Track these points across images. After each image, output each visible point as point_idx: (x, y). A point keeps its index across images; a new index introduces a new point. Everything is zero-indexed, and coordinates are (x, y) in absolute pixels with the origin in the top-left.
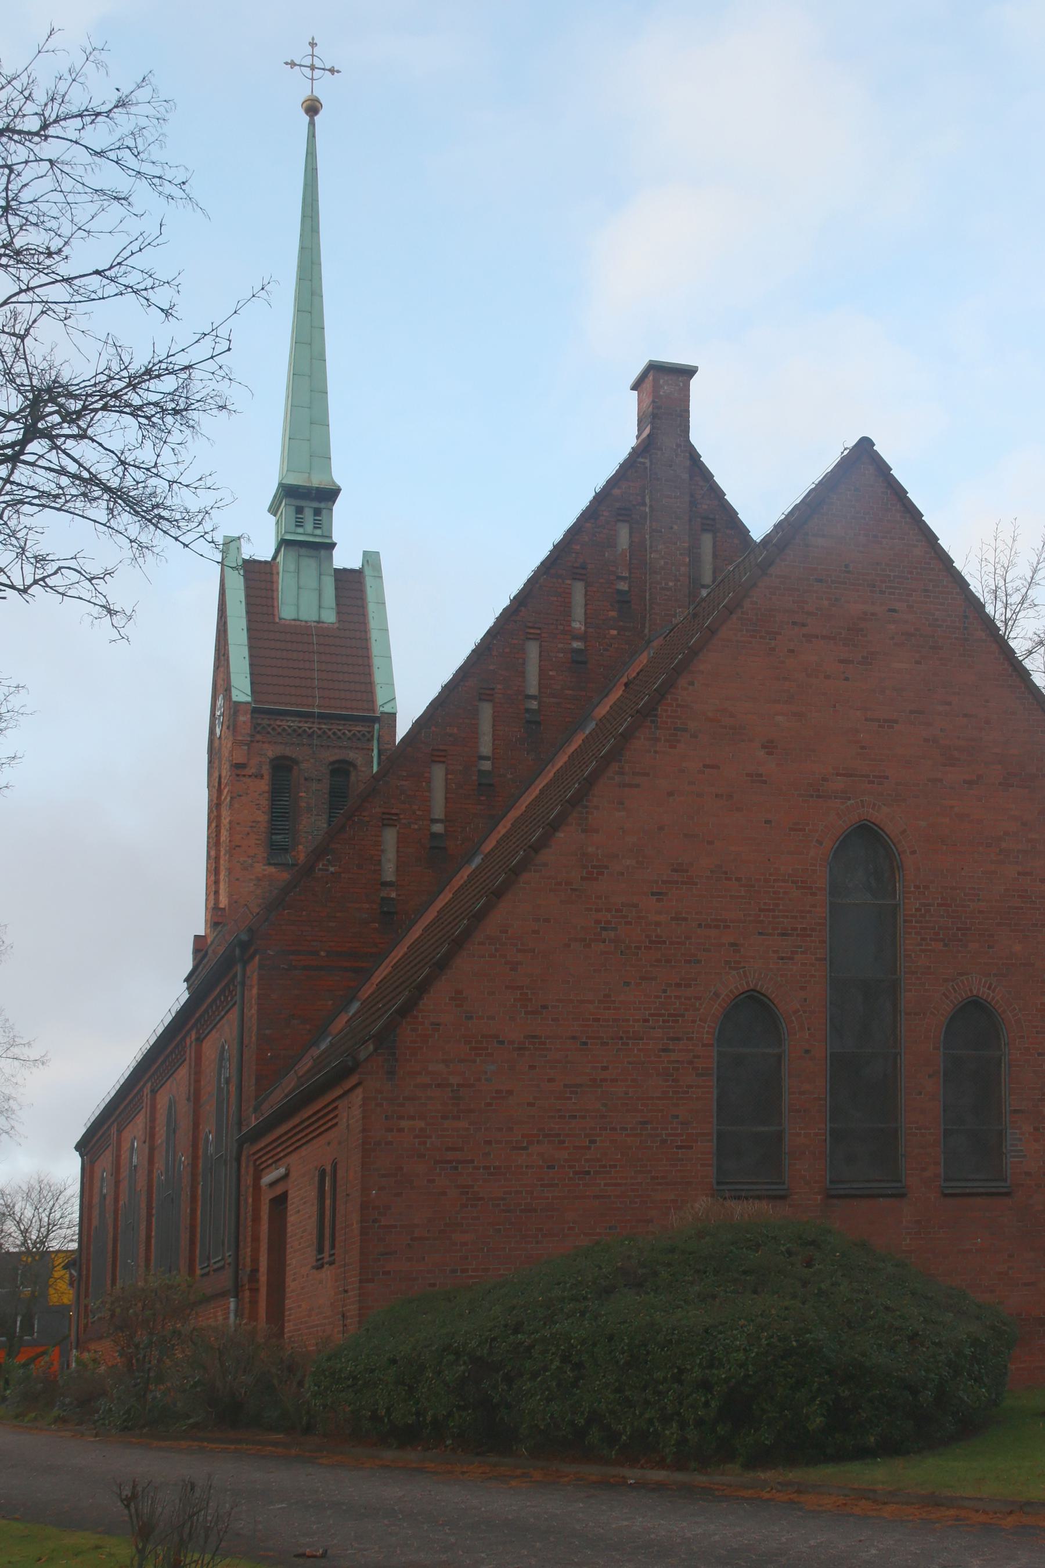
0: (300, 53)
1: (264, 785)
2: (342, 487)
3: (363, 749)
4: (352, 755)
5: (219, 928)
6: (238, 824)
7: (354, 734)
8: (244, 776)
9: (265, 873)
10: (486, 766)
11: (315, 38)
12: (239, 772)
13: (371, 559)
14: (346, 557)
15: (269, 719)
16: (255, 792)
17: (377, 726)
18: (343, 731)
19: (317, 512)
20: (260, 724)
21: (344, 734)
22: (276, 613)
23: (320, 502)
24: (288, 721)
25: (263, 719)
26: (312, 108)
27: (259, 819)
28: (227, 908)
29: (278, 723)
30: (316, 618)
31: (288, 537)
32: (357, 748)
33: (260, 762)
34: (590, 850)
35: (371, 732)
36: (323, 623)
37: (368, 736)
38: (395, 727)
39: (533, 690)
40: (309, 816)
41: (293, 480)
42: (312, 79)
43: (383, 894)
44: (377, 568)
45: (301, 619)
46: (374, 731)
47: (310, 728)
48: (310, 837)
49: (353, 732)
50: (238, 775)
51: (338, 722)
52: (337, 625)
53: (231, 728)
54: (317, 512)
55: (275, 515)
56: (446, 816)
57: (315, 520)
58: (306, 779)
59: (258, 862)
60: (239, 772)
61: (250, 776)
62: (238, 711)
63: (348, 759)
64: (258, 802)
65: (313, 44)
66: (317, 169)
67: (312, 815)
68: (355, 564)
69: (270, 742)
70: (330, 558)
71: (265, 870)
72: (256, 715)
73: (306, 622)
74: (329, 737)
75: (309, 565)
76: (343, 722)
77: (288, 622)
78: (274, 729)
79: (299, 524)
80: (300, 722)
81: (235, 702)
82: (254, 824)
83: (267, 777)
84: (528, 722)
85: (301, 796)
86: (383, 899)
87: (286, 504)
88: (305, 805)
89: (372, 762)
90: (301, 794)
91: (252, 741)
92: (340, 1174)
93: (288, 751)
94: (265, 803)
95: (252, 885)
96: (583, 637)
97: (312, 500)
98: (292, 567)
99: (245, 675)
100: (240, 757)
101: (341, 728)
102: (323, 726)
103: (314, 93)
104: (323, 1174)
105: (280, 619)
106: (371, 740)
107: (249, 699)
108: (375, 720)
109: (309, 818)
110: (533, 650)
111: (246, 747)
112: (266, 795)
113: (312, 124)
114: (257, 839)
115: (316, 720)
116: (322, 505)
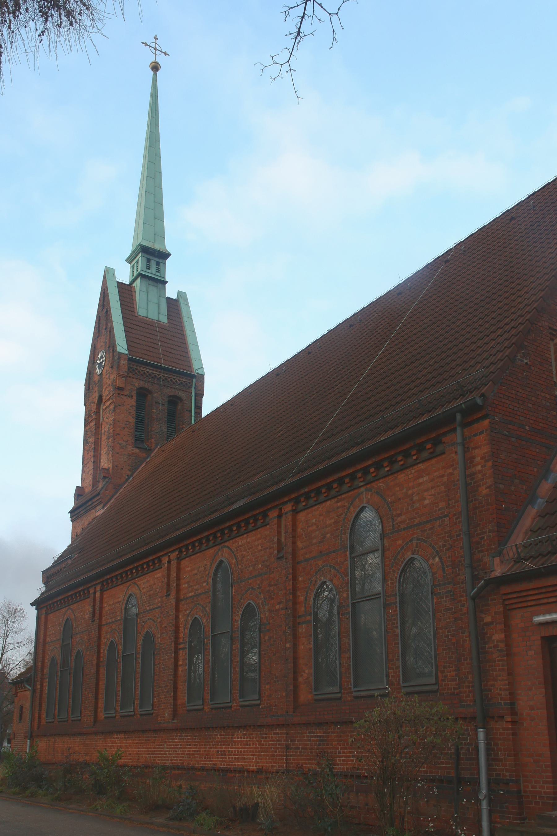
0: (150, 40)
1: (132, 402)
2: (171, 253)
3: (186, 391)
4: (180, 394)
5: (107, 480)
6: (118, 421)
7: (181, 383)
8: (122, 395)
9: (133, 452)
11: (142, 41)
12: (119, 392)
14: (171, 292)
15: (137, 366)
16: (128, 405)
17: (194, 380)
18: (176, 380)
19: (158, 264)
20: (131, 368)
21: (176, 381)
22: (136, 311)
23: (159, 259)
24: (147, 369)
25: (133, 365)
26: (155, 68)
27: (130, 421)
28: (111, 469)
29: (142, 369)
30: (157, 319)
31: (143, 273)
32: (183, 391)
33: (131, 388)
35: (191, 383)
36: (161, 322)
37: (189, 385)
38: (204, 382)
40: (157, 423)
41: (145, 243)
42: (155, 54)
44: (186, 300)
45: (149, 317)
46: (192, 383)
47: (159, 375)
48: (158, 435)
49: (181, 381)
50: (119, 394)
51: (173, 374)
52: (168, 325)
53: (115, 367)
54: (158, 264)
55: (130, 263)
57: (156, 267)
58: (156, 403)
59: (129, 445)
60: (119, 392)
61: (125, 395)
62: (121, 358)
63: (178, 395)
64: (129, 411)
65: (156, 38)
67: (159, 423)
68: (174, 297)
69: (137, 379)
70: (164, 288)
71: (133, 450)
72: (130, 362)
73: (152, 319)
74: (168, 381)
75: (153, 290)
76: (176, 375)
77: (142, 318)
78: (139, 372)
79: (148, 268)
80: (153, 370)
81: (119, 352)
82: (127, 423)
83: (135, 397)
85: (154, 412)
87: (142, 256)
88: (155, 417)
89: (191, 399)
90: (153, 411)
91: (127, 376)
93: (146, 385)
94: (134, 412)
95: (126, 457)
97: (155, 257)
98: (144, 289)
99: (123, 339)
100: (120, 383)
101: (175, 378)
102: (166, 375)
103: (156, 60)
105: (138, 315)
106: (191, 387)
107: (127, 352)
108: (192, 376)
109: (157, 424)
111: (124, 379)
112: (135, 408)
113: (155, 75)
114: (129, 432)
115: (162, 371)
116: (160, 261)
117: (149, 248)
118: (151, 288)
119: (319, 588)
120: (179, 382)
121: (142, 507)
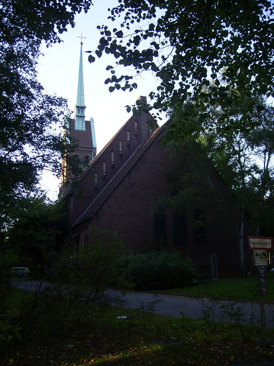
4: (88, 155)
10: (113, 163)
13: (92, 119)
14: (87, 119)
17: (93, 149)
19: (82, 111)
30: (82, 129)
34: (131, 182)
39: (121, 150)
43: (95, 186)
44: (93, 121)
54: (82, 111)
56: (106, 172)
66: (83, 79)
75: (81, 120)
84: (120, 156)
86: (95, 186)
92: (89, 237)
96: (130, 141)
97: (81, 108)
98: (77, 120)
104: (85, 236)
108: (93, 148)
110: (121, 144)
113: (81, 46)
116: (83, 109)
117: (79, 106)
118: (80, 119)
119: (264, 266)
120: (88, 151)
121: (95, 206)
